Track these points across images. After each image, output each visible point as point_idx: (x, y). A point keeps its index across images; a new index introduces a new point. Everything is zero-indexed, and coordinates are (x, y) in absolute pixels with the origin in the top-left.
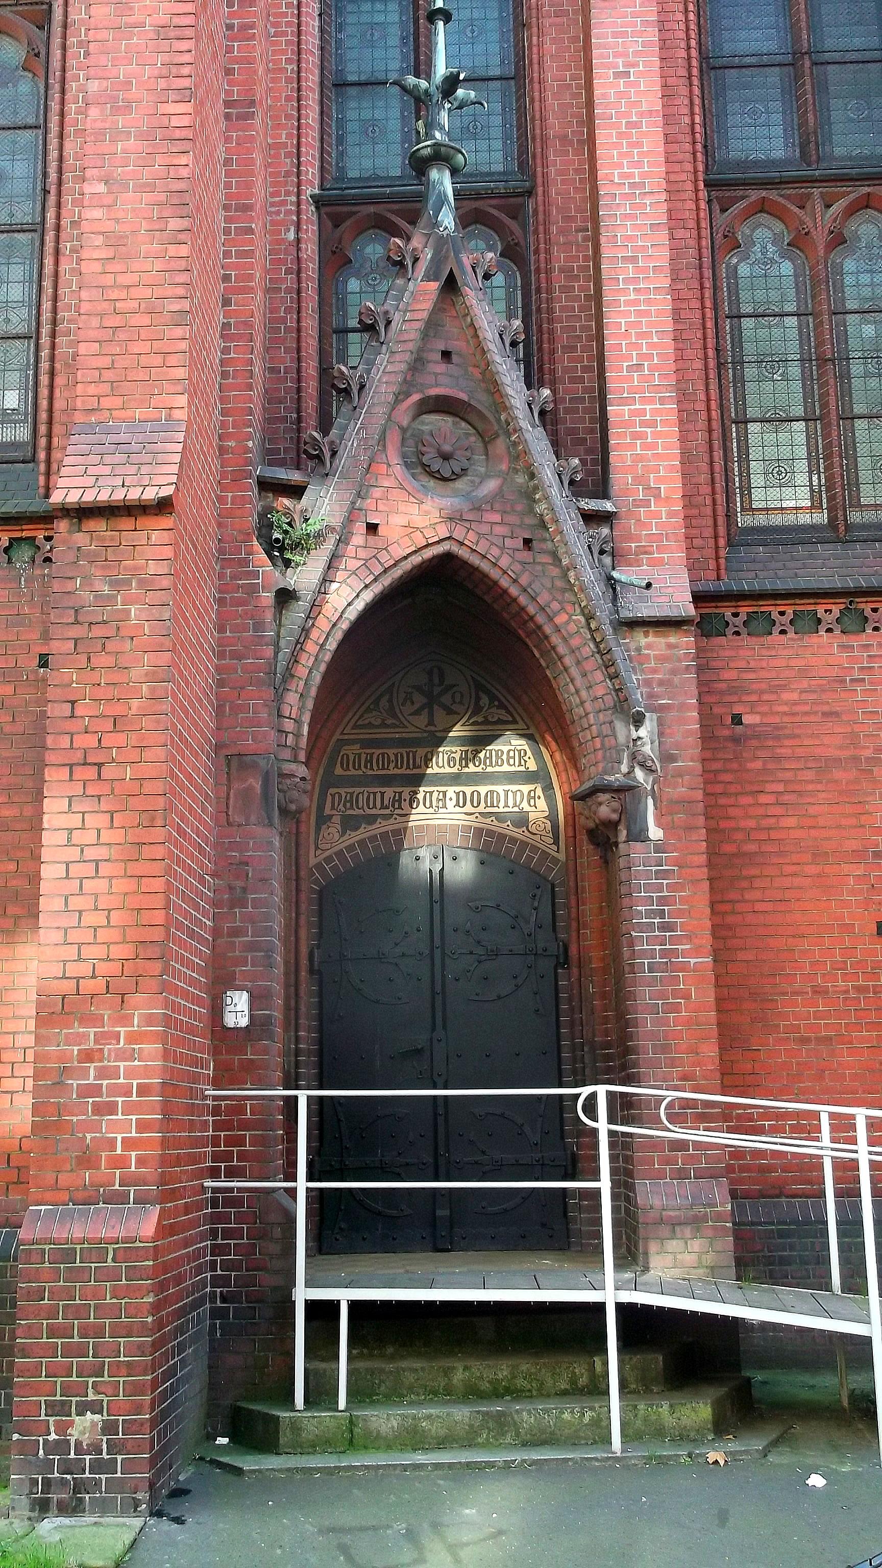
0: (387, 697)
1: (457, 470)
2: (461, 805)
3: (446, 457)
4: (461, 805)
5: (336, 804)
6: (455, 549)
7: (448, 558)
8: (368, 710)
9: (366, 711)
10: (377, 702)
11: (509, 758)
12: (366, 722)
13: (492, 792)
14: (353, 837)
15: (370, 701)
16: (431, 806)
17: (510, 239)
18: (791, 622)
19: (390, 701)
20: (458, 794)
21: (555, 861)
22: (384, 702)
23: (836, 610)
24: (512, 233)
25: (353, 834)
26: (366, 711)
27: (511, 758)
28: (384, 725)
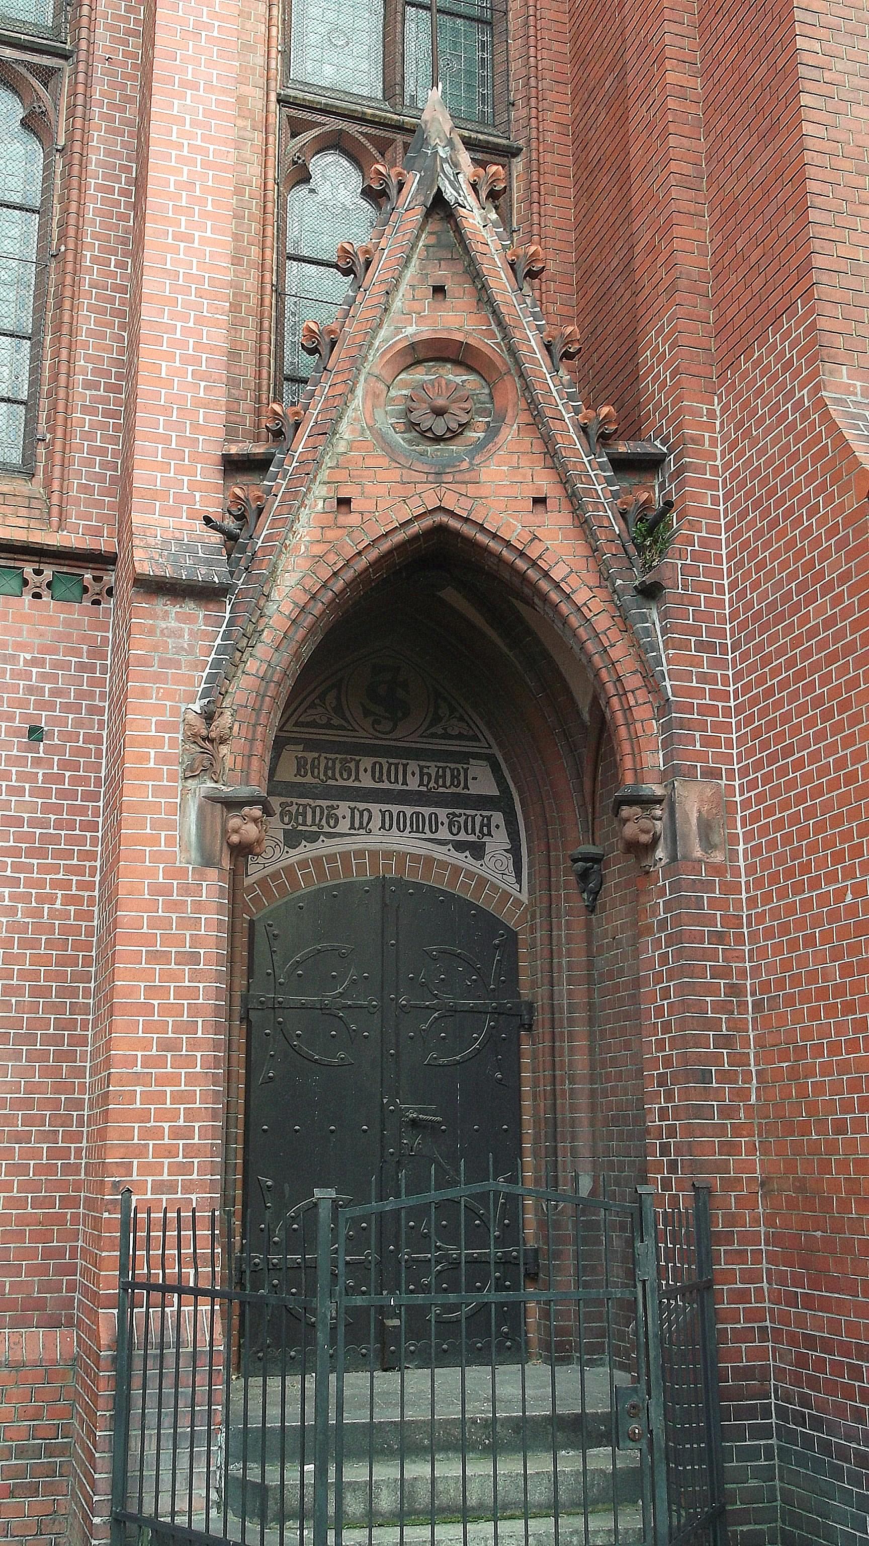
0: (334, 693)
1: (454, 426)
2: (387, 827)
3: (439, 412)
4: (387, 827)
5: (317, 819)
6: (445, 519)
7: (440, 530)
8: (313, 706)
9: (309, 707)
10: (322, 697)
11: (313, 767)
12: (309, 719)
13: (418, 814)
14: (295, 855)
15: (313, 696)
16: (473, 832)
17: (35, 105)
18: (49, 585)
19: (338, 699)
20: (353, 810)
21: (518, 903)
22: (331, 698)
23: (48, 573)
24: (39, 99)
25: (470, 859)
26: (309, 707)
27: (330, 769)
28: (328, 726)
